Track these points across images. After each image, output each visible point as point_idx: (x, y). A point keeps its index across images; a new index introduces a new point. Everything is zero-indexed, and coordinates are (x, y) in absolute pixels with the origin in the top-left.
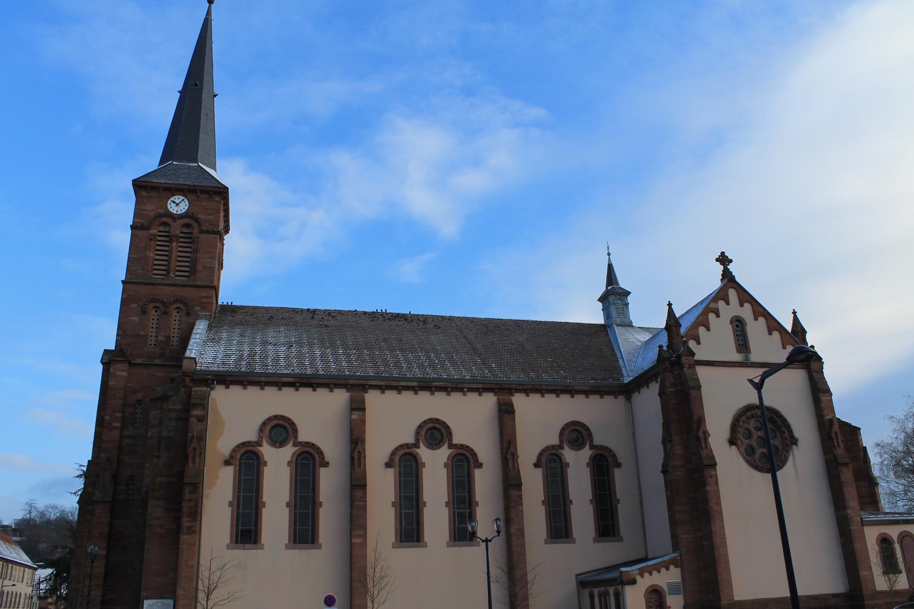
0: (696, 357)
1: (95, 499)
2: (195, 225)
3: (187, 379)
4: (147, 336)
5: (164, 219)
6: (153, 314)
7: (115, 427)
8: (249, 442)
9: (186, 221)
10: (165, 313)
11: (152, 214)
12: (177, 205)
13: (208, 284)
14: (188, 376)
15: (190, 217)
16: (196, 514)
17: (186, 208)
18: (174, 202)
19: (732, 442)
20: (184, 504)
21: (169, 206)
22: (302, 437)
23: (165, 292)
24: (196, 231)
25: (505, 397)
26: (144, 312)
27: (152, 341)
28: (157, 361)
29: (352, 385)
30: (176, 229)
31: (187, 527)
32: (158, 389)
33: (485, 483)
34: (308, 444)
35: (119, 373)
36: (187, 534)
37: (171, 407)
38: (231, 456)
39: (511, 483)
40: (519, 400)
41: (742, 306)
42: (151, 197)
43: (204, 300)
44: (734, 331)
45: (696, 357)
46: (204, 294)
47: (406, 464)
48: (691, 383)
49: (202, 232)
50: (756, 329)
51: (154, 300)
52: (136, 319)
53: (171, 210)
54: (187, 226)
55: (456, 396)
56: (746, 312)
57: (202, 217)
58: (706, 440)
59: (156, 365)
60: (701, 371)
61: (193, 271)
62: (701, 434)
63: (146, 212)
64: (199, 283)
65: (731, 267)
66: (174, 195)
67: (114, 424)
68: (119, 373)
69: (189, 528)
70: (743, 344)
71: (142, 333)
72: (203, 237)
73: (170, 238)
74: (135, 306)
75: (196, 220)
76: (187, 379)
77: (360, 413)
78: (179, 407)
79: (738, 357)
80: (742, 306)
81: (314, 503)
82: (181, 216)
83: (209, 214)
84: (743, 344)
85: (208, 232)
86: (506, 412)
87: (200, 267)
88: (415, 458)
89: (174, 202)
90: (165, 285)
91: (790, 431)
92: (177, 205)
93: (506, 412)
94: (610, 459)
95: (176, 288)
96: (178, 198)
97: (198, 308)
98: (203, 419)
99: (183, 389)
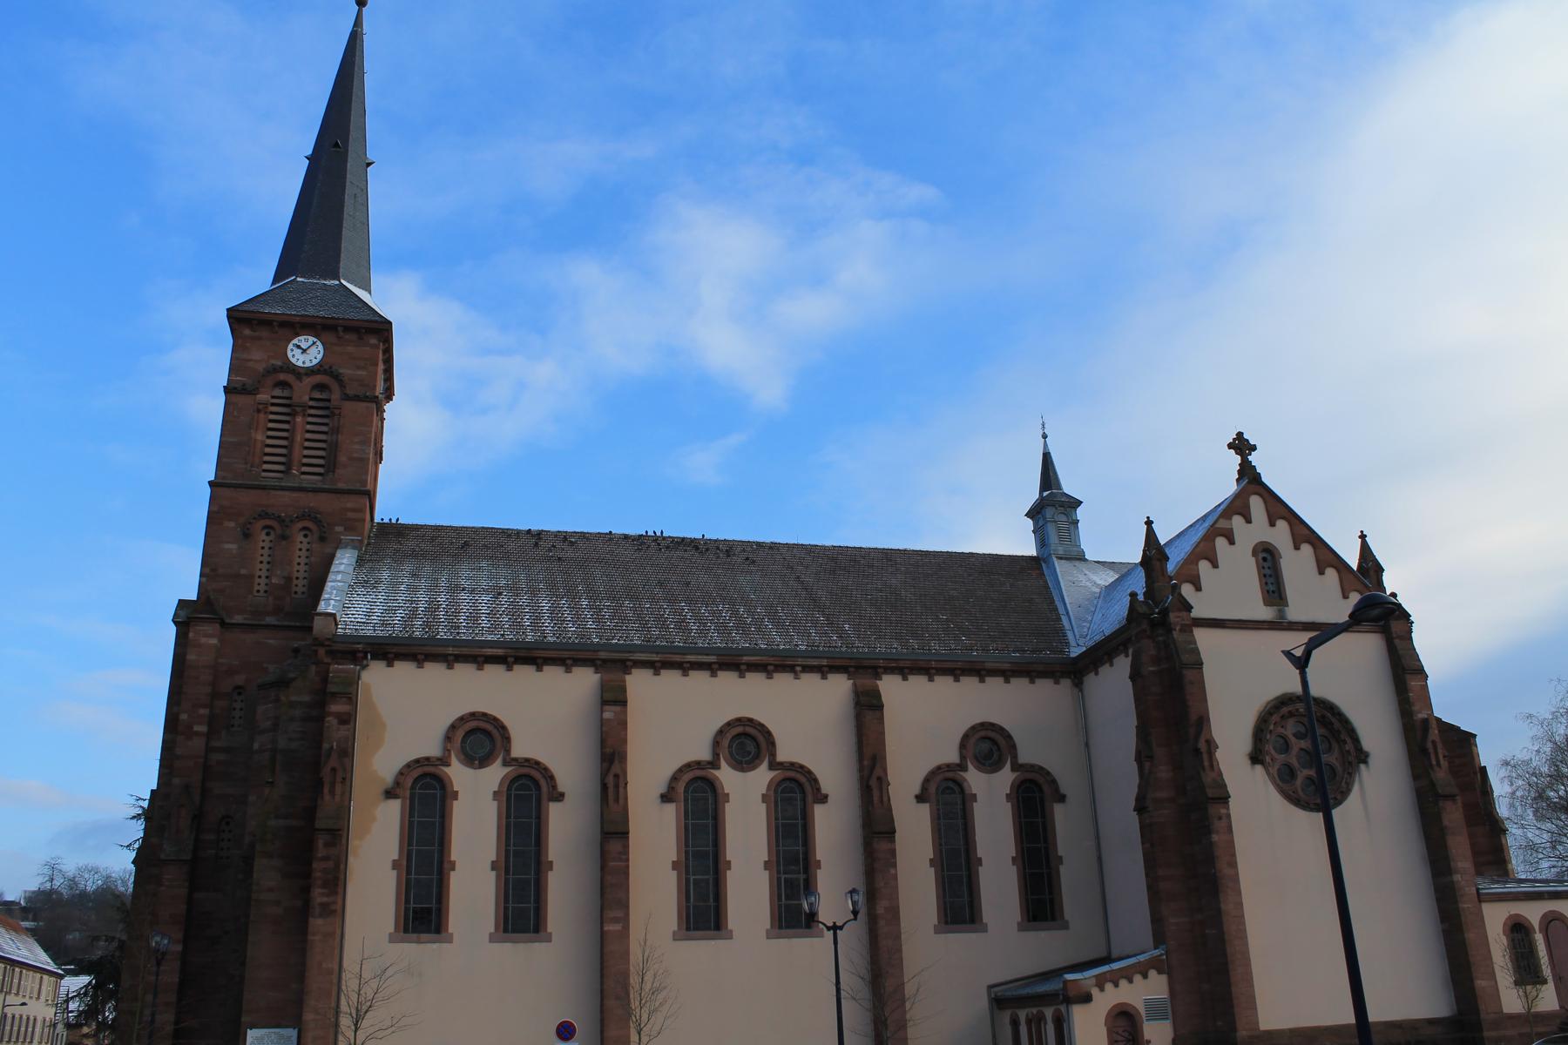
0: (1195, 613)
1: (163, 856)
2: (335, 386)
3: (322, 651)
4: (251, 577)
5: (282, 377)
6: (263, 539)
7: (198, 734)
8: (427, 759)
9: (318, 379)
10: (284, 537)
11: (261, 368)
12: (304, 351)
13: (358, 487)
14: (322, 645)
15: (325, 372)
16: (336, 882)
17: (320, 357)
18: (299, 347)
19: (1256, 758)
20: (315, 865)
21: (290, 354)
22: (518, 751)
23: (283, 501)
24: (336, 396)
25: (866, 682)
26: (247, 535)
27: (260, 584)
28: (270, 620)
29: (604, 661)
30: (302, 392)
31: (321, 904)
32: (271, 668)
33: (833, 829)
34: (529, 762)
35: (203, 640)
36: (321, 916)
37: (294, 698)
38: (397, 783)
39: (876, 829)
40: (890, 687)
41: (1272, 524)
42: (260, 338)
43: (350, 515)
44: (1260, 568)
45: (1195, 613)
46: (349, 505)
47: (697, 796)
48: (1185, 658)
49: (347, 398)
50: (1296, 565)
51: (264, 515)
52: (233, 546)
53: (293, 360)
54: (321, 387)
55: (783, 680)
56: (1280, 536)
57: (346, 372)
58: (1211, 754)
59: (267, 626)
60: (1203, 637)
61: (331, 465)
62: (1202, 745)
63: (250, 364)
64: (341, 485)
65: (1253, 458)
66: (298, 335)
67: (196, 728)
68: (203, 640)
69: (324, 906)
70: (1274, 591)
71: (243, 571)
72: (349, 406)
73: (292, 409)
74: (232, 524)
75: (337, 377)
76: (322, 651)
77: (618, 708)
78: (306, 698)
79: (1266, 613)
80: (1272, 524)
81: (538, 862)
82: (311, 371)
83: (358, 368)
84: (1274, 591)
85: (357, 398)
86: (867, 707)
87: (342, 458)
88: (711, 786)
89: (299, 347)
90: (283, 489)
91: (1356, 740)
92: (304, 351)
93: (867, 707)
94: (1046, 788)
95: (295, 495)
96: (305, 340)
97: (339, 529)
98: (348, 719)
99: (313, 668)
